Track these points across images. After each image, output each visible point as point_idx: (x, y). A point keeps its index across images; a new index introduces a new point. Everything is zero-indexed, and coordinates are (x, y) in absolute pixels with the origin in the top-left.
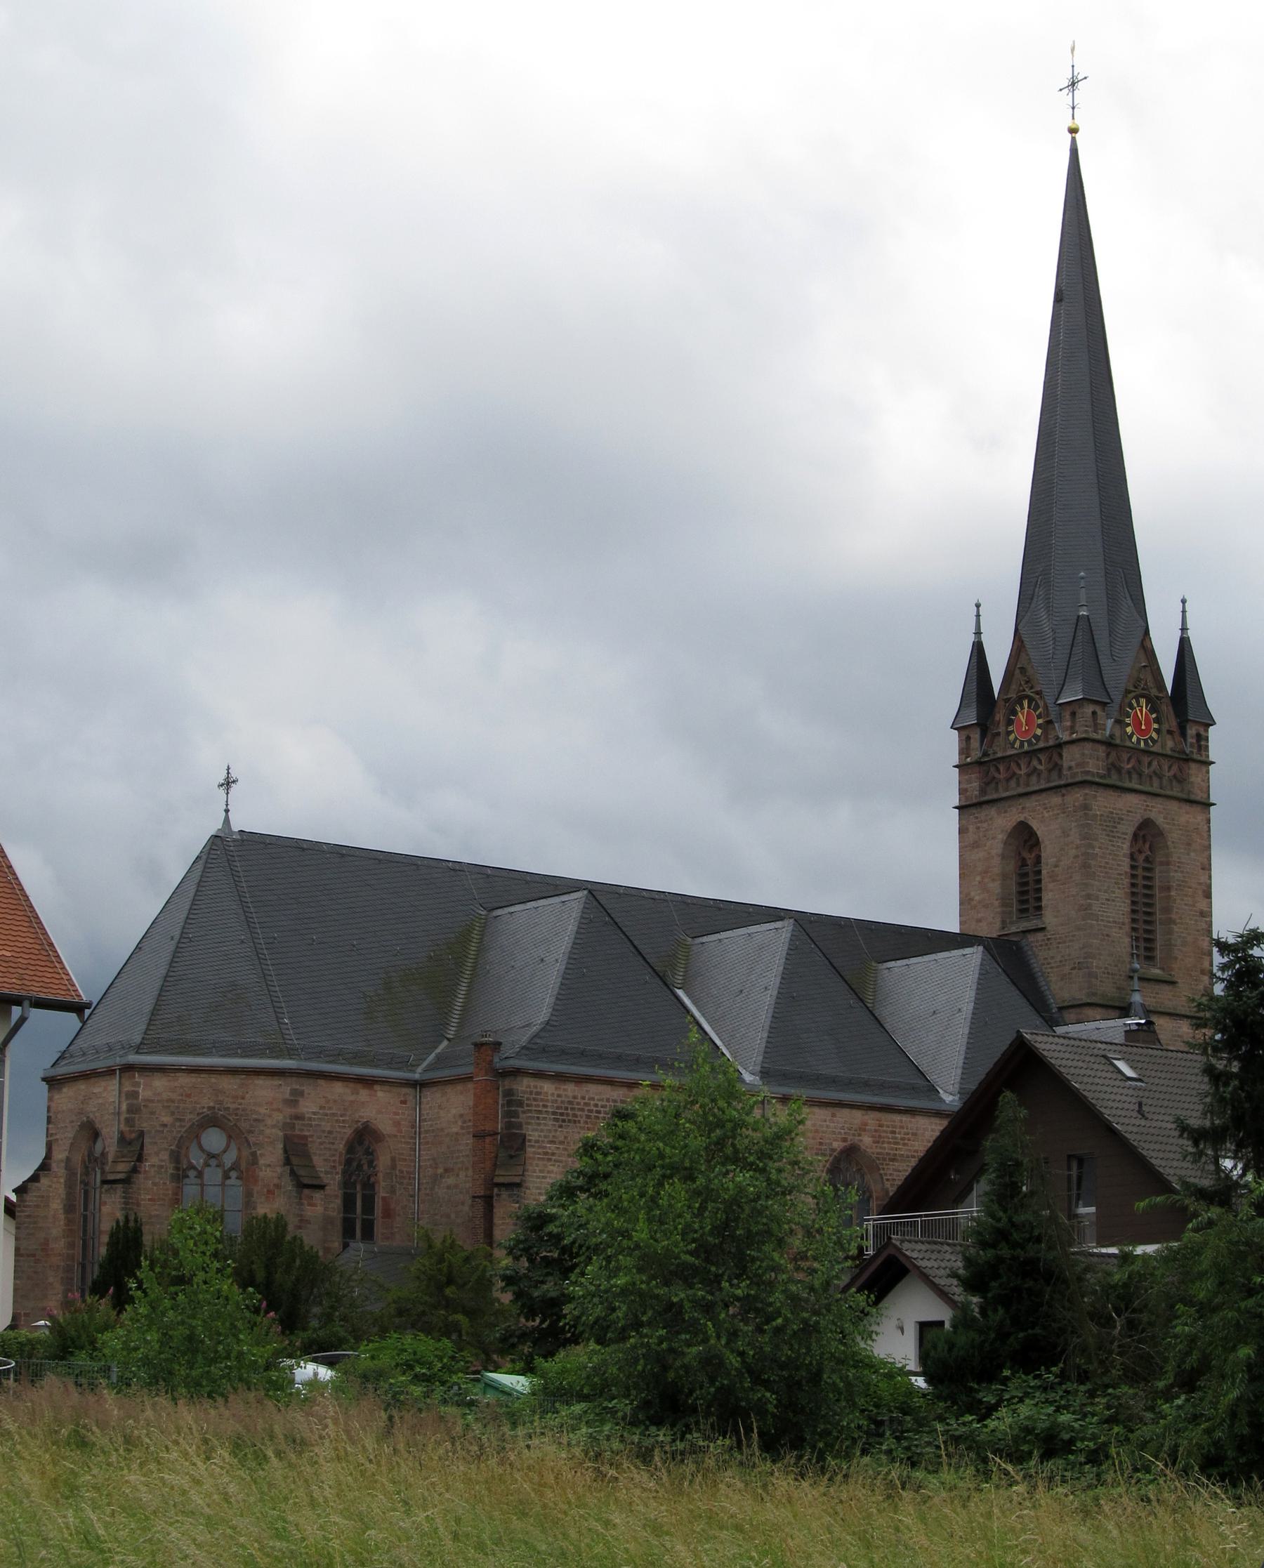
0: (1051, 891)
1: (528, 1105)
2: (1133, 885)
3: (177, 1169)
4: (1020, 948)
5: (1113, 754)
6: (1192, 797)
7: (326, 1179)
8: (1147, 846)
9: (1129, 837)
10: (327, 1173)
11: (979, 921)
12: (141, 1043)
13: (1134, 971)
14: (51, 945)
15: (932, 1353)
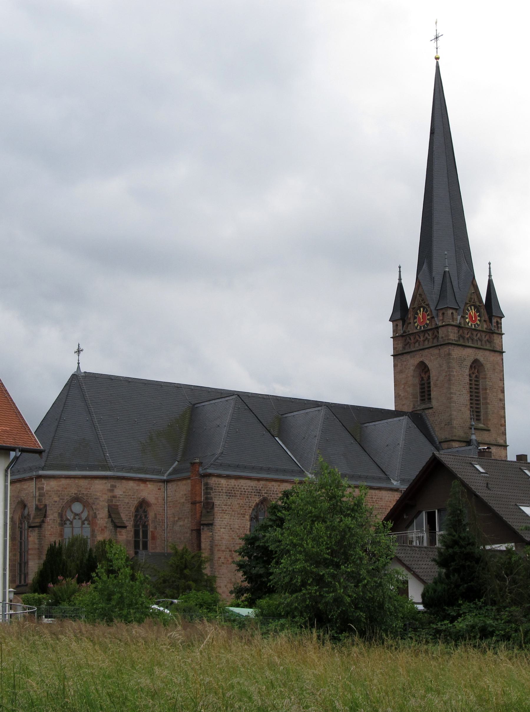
0: (435, 391)
1: (215, 489)
2: (471, 388)
3: (62, 520)
4: (422, 417)
5: (461, 331)
6: (495, 349)
7: (127, 524)
8: (476, 370)
9: (469, 367)
10: (127, 521)
11: (404, 405)
12: (45, 466)
13: (472, 425)
14: (26, 424)
15: (427, 594)
